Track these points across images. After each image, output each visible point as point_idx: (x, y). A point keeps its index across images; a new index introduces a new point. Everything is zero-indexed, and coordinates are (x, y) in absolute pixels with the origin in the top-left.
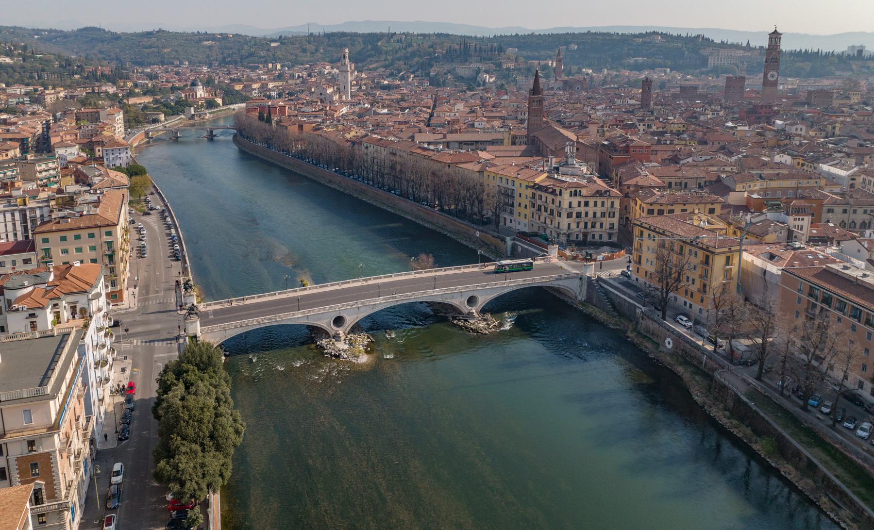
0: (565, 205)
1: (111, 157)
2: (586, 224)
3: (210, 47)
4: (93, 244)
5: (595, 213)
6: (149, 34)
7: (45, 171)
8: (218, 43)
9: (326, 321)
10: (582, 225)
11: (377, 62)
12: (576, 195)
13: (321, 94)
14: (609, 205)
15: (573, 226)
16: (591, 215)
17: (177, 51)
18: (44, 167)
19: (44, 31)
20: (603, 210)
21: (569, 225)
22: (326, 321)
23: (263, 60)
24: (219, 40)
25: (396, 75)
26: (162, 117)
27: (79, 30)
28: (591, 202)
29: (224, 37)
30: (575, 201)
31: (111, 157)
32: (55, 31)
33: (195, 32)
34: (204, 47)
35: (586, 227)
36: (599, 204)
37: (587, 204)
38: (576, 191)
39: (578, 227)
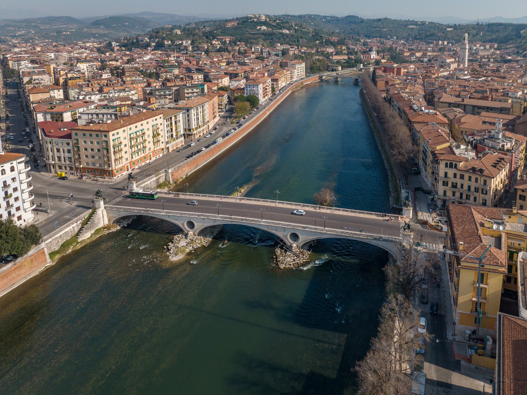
0: (441, 174)
1: (249, 89)
2: (461, 194)
3: (412, 29)
4: (98, 141)
5: (469, 187)
6: (379, 20)
7: (191, 93)
8: (418, 27)
9: (182, 222)
10: (458, 195)
11: (513, 43)
12: (451, 166)
13: (442, 62)
14: (482, 183)
15: (449, 194)
16: (466, 187)
17: (391, 31)
18: (190, 91)
19: (329, 17)
20: (477, 185)
21: (445, 192)
22: (182, 222)
23: (437, 38)
24: (419, 25)
25: (521, 53)
26: (340, 68)
27: (346, 17)
28: (466, 176)
29: (423, 23)
30: (451, 172)
31: (249, 89)
32: (334, 17)
33: (407, 20)
34: (409, 29)
35: (461, 197)
36: (473, 179)
37: (462, 177)
38: (451, 163)
39: (454, 195)
